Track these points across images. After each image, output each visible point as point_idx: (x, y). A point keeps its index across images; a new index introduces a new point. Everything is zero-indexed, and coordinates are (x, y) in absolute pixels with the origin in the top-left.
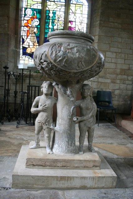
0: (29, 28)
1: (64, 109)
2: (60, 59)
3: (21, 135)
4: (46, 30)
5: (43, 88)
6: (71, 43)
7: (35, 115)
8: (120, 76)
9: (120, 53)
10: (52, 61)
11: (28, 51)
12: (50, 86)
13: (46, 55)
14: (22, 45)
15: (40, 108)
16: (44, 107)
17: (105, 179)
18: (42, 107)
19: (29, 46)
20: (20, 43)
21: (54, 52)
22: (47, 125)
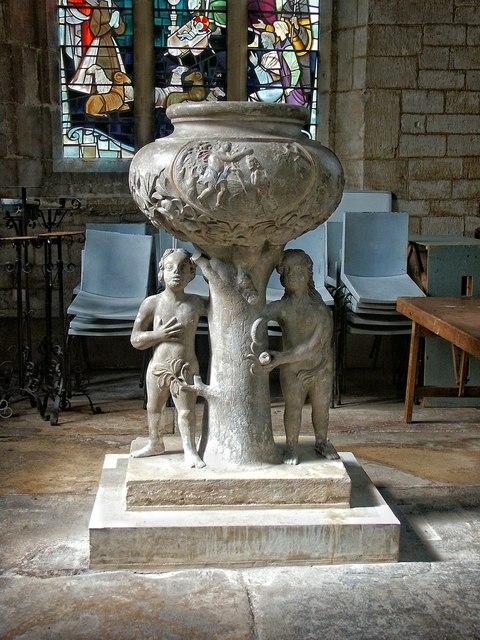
0: (88, 11)
1: (230, 330)
2: (207, 190)
3: (92, 430)
4: (159, 17)
5: (163, 269)
6: (234, 140)
7: (147, 354)
8: (466, 183)
9: (460, 90)
10: (186, 198)
11: (94, 108)
12: (186, 269)
13: (167, 180)
14: (67, 84)
15: (159, 330)
16: (172, 327)
17: (361, 533)
18: (163, 326)
19: (94, 85)
20: (57, 78)
21: (189, 173)
22: (181, 380)
